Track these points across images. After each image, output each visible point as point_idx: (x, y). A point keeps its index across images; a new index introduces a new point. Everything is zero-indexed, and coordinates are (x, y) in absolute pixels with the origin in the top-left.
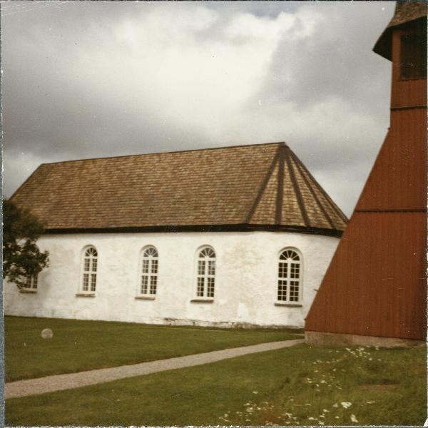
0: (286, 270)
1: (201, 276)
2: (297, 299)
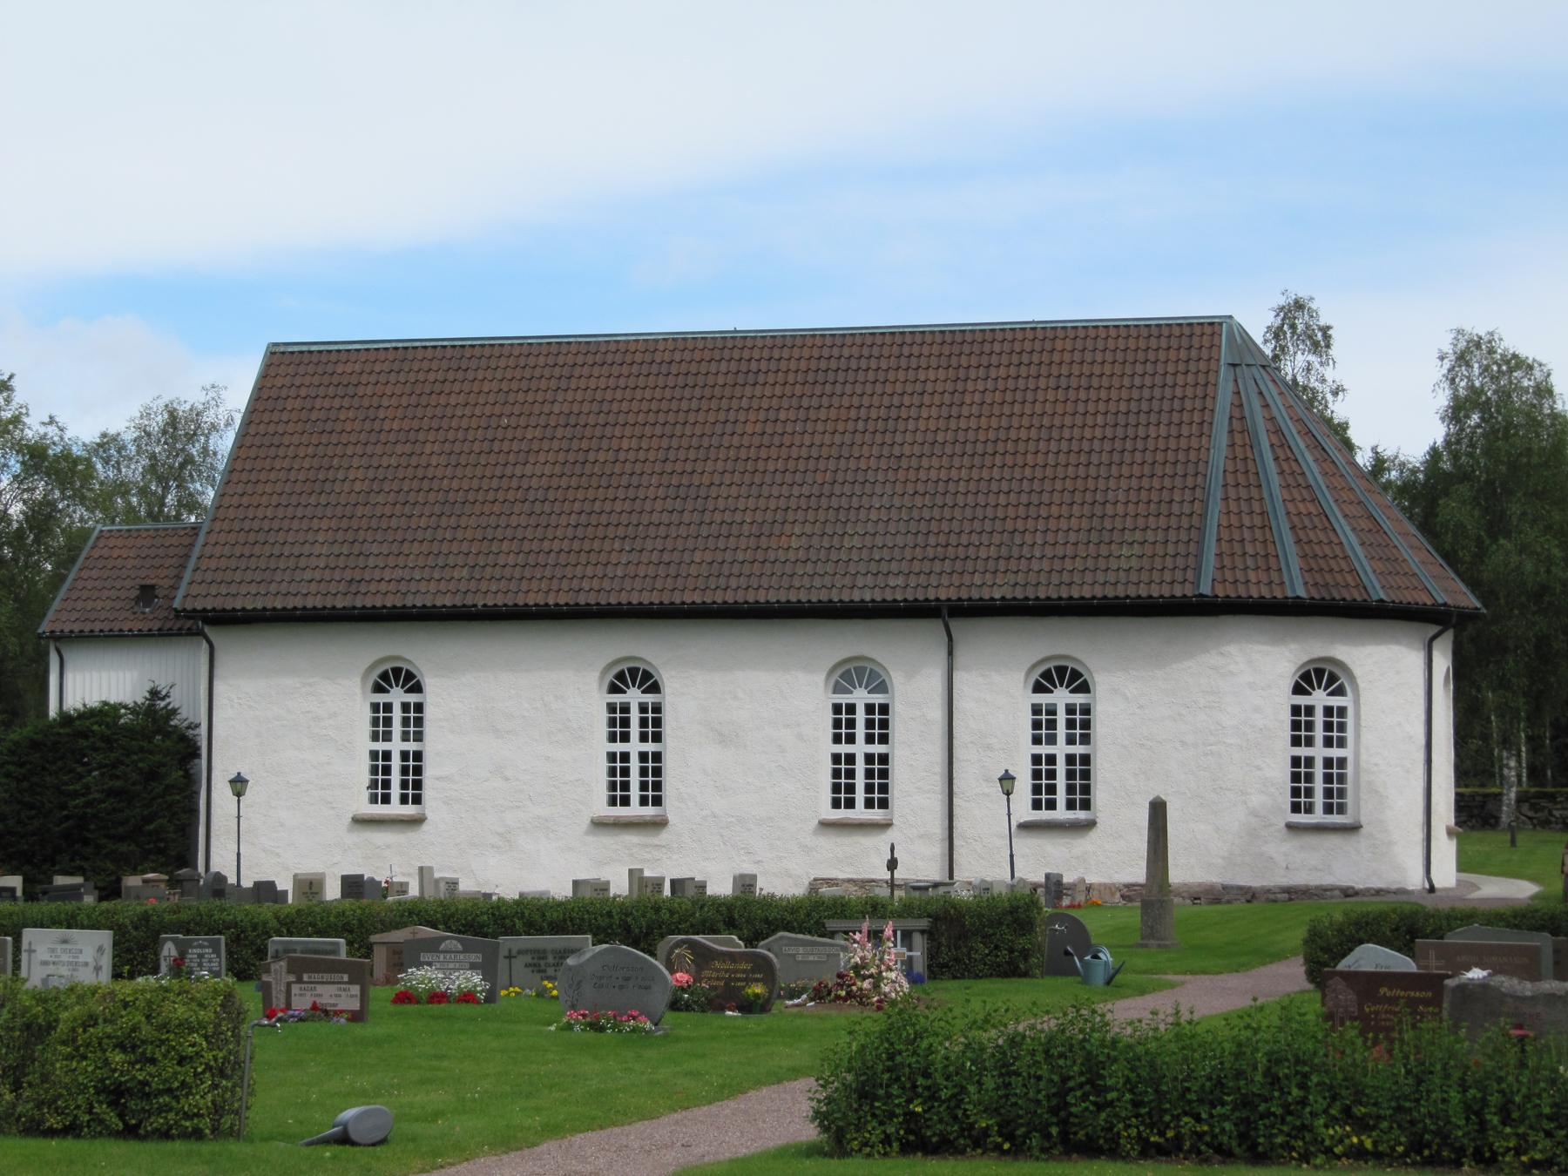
0: (870, 724)
1: (381, 746)
2: (1342, 809)
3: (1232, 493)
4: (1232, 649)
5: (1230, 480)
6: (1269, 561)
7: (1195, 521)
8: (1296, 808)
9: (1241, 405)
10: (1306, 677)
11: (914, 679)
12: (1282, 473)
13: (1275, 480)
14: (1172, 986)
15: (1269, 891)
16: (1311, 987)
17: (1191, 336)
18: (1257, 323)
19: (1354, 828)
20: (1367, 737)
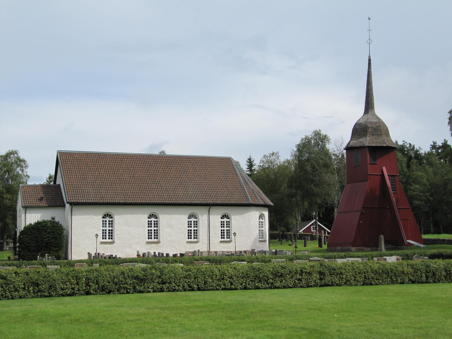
11: (203, 217)
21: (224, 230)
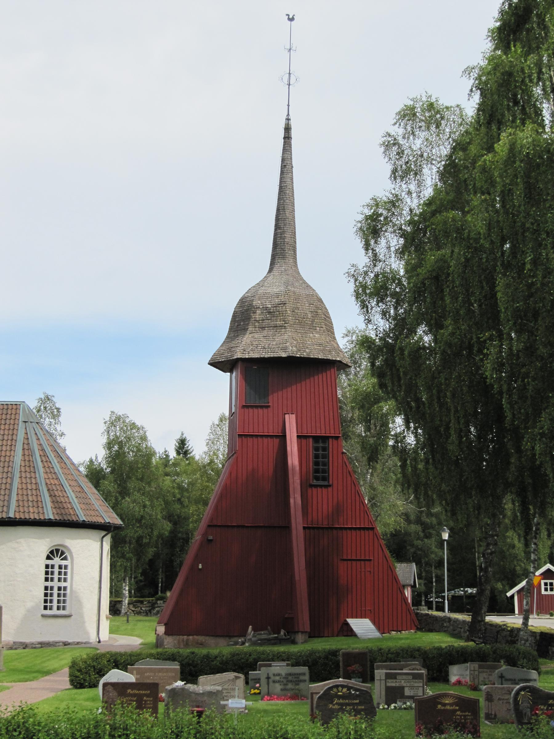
2: (64, 608)
3: (23, 475)
4: (22, 540)
5: (23, 470)
6: (38, 503)
7: (8, 486)
8: (45, 608)
9: (28, 439)
10: (52, 552)
12: (44, 467)
13: (42, 470)
14: (8, 688)
15: (33, 644)
16: (71, 687)
17: (7, 409)
18: (33, 404)
19: (69, 616)
20: (76, 578)
21: (52, 588)
